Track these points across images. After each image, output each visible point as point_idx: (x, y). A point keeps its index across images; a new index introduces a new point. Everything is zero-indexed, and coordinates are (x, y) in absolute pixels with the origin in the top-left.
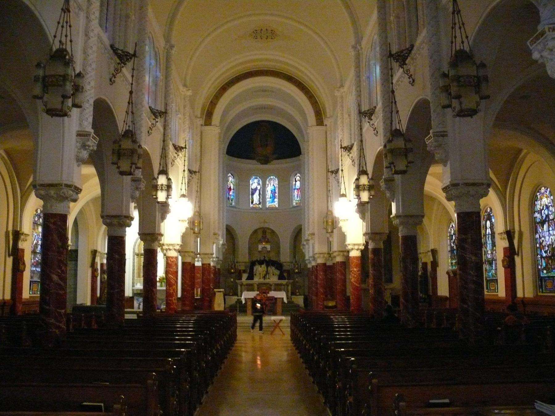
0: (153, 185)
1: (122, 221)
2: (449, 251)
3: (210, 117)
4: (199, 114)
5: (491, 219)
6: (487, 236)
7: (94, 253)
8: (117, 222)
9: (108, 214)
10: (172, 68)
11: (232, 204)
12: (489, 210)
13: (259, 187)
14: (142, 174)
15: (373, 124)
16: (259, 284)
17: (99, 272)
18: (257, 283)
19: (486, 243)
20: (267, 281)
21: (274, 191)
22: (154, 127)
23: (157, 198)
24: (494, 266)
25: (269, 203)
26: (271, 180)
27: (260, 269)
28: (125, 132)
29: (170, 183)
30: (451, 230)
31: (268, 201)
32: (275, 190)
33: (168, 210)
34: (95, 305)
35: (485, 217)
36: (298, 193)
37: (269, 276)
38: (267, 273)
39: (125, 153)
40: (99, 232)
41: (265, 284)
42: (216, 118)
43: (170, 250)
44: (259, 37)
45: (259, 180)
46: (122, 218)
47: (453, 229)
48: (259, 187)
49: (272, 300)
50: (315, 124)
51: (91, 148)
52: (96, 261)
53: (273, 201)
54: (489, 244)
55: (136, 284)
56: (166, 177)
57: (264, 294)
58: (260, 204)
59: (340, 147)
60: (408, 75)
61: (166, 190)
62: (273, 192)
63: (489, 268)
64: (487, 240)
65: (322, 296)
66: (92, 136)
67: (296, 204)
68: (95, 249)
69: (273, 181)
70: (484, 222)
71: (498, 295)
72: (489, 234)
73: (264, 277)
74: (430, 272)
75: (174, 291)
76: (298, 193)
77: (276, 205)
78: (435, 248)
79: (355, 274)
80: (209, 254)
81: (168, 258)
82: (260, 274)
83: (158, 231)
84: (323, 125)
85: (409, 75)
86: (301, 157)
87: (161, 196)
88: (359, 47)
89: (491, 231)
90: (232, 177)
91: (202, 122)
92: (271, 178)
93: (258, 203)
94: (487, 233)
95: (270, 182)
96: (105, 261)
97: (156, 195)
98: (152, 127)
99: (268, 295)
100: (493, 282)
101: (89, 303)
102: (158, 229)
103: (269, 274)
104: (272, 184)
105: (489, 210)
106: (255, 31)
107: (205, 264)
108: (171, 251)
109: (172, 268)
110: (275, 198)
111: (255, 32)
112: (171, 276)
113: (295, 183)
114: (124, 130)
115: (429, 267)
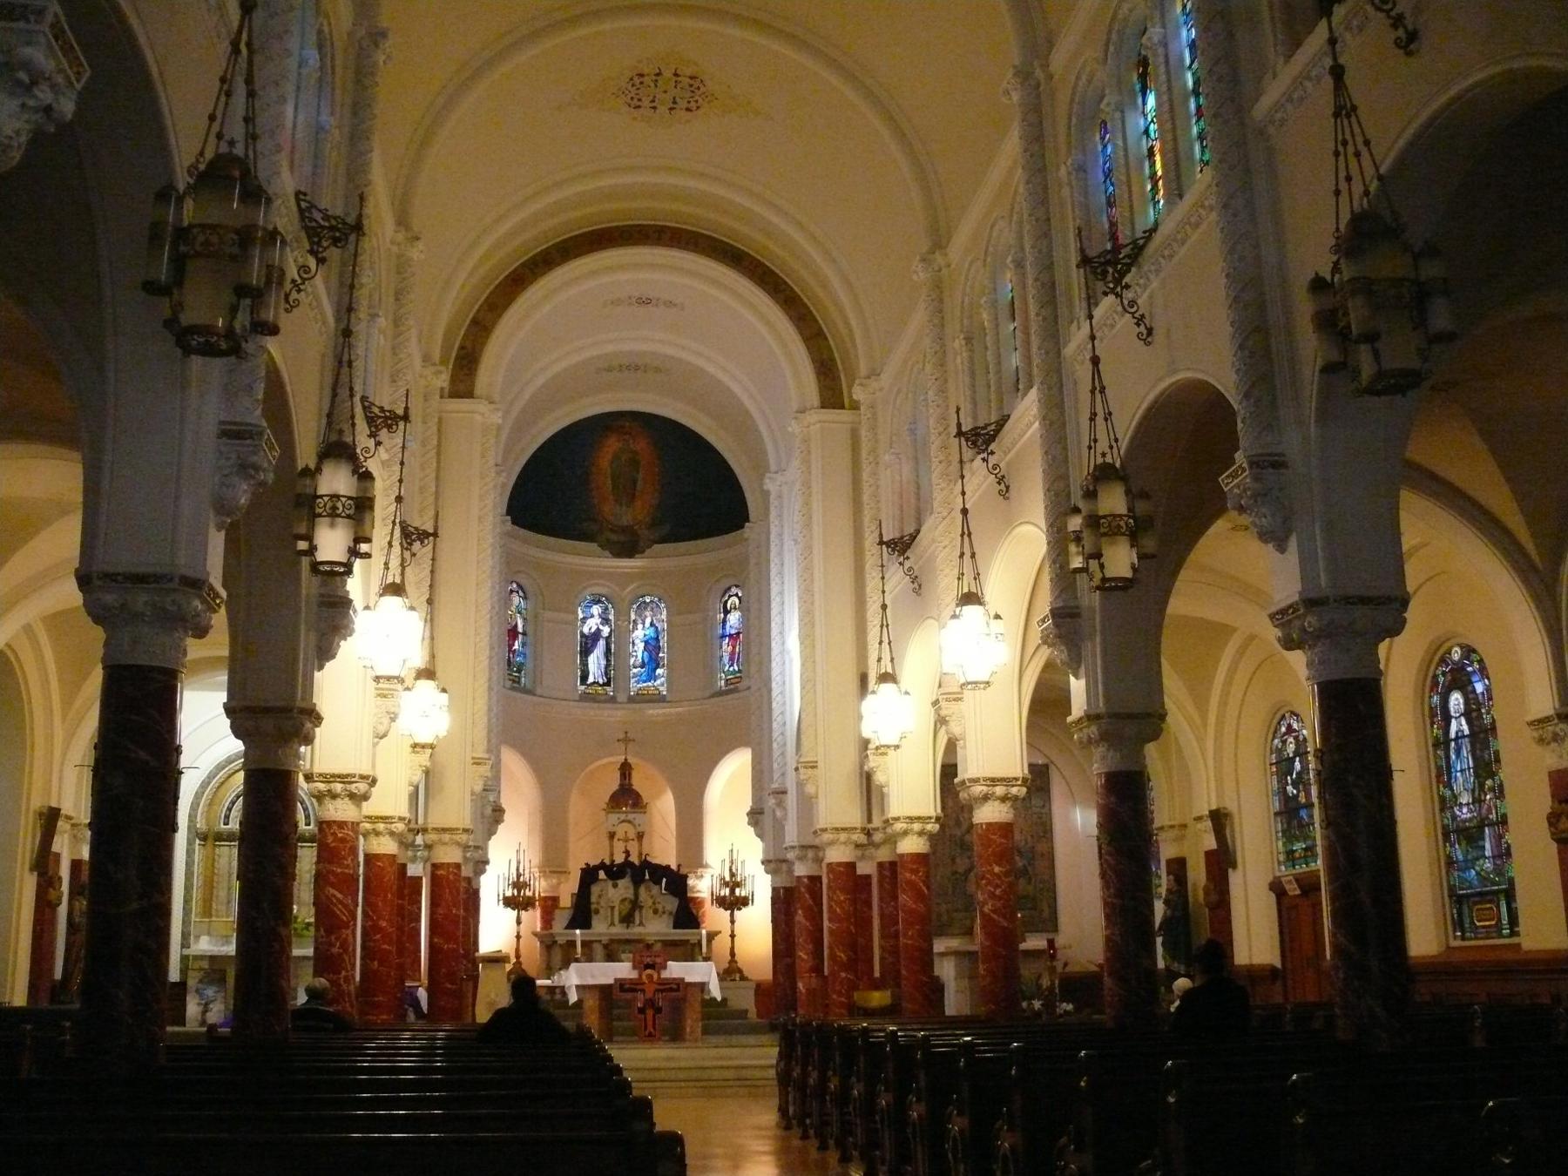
0: (299, 495)
1: (173, 601)
2: (1276, 814)
3: (470, 369)
4: (437, 355)
5: (1471, 683)
6: (1453, 744)
7: (50, 819)
8: (146, 603)
9: (111, 569)
10: (375, 112)
11: (519, 683)
12: (1456, 655)
13: (606, 630)
14: (265, 414)
15: (1132, 303)
16: (612, 941)
17: (65, 888)
18: (605, 940)
19: (1449, 767)
20: (636, 931)
21: (653, 643)
22: (310, 279)
23: (312, 550)
24: (1488, 846)
25: (638, 682)
26: (645, 608)
27: (612, 894)
28: (211, 164)
29: (366, 490)
30: (1284, 742)
31: (635, 675)
32: (657, 639)
33: (345, 622)
34: (44, 1004)
35: (1441, 679)
36: (734, 647)
37: (641, 916)
38: (635, 905)
39: (207, 243)
40: (70, 736)
41: (628, 941)
42: (489, 372)
43: (334, 796)
44: (646, 102)
45: (607, 609)
46: (171, 585)
47: (1291, 739)
48: (606, 630)
49: (678, 990)
50: (816, 401)
51: (44, 95)
52: (55, 848)
53: (652, 676)
54: (1462, 771)
55: (197, 937)
56: (351, 468)
57: (649, 971)
58: (608, 684)
59: (954, 431)
60: (1389, 17)
61: (349, 517)
62: (652, 646)
63: (1466, 853)
64: (1453, 757)
65: (843, 975)
66: (49, 18)
67: (726, 685)
68: (54, 804)
69: (652, 610)
70: (1436, 699)
71: (1519, 945)
72: (1464, 737)
73: (627, 919)
74: (1205, 886)
75: (346, 951)
76: (734, 647)
77: (661, 689)
78: (1221, 806)
79: (997, 886)
80: (458, 829)
81: (324, 826)
82: (613, 908)
83: (303, 699)
84: (843, 407)
85: (1393, 13)
86: (748, 531)
87: (331, 543)
88: (1039, 73)
89: (1469, 722)
90: (521, 594)
91: (443, 380)
92: (645, 602)
93: (601, 682)
94: (1453, 735)
95: (640, 616)
96: (85, 854)
97: (309, 537)
98: (299, 281)
99: (665, 974)
100: (1490, 902)
101: (19, 999)
102: (304, 692)
103: (641, 907)
104: (648, 621)
105: (1456, 655)
106: (636, 79)
107: (443, 864)
108: (339, 801)
109: (340, 865)
110: (658, 666)
111: (637, 81)
112: (336, 893)
113: (722, 615)
114: (209, 154)
115: (1197, 874)
